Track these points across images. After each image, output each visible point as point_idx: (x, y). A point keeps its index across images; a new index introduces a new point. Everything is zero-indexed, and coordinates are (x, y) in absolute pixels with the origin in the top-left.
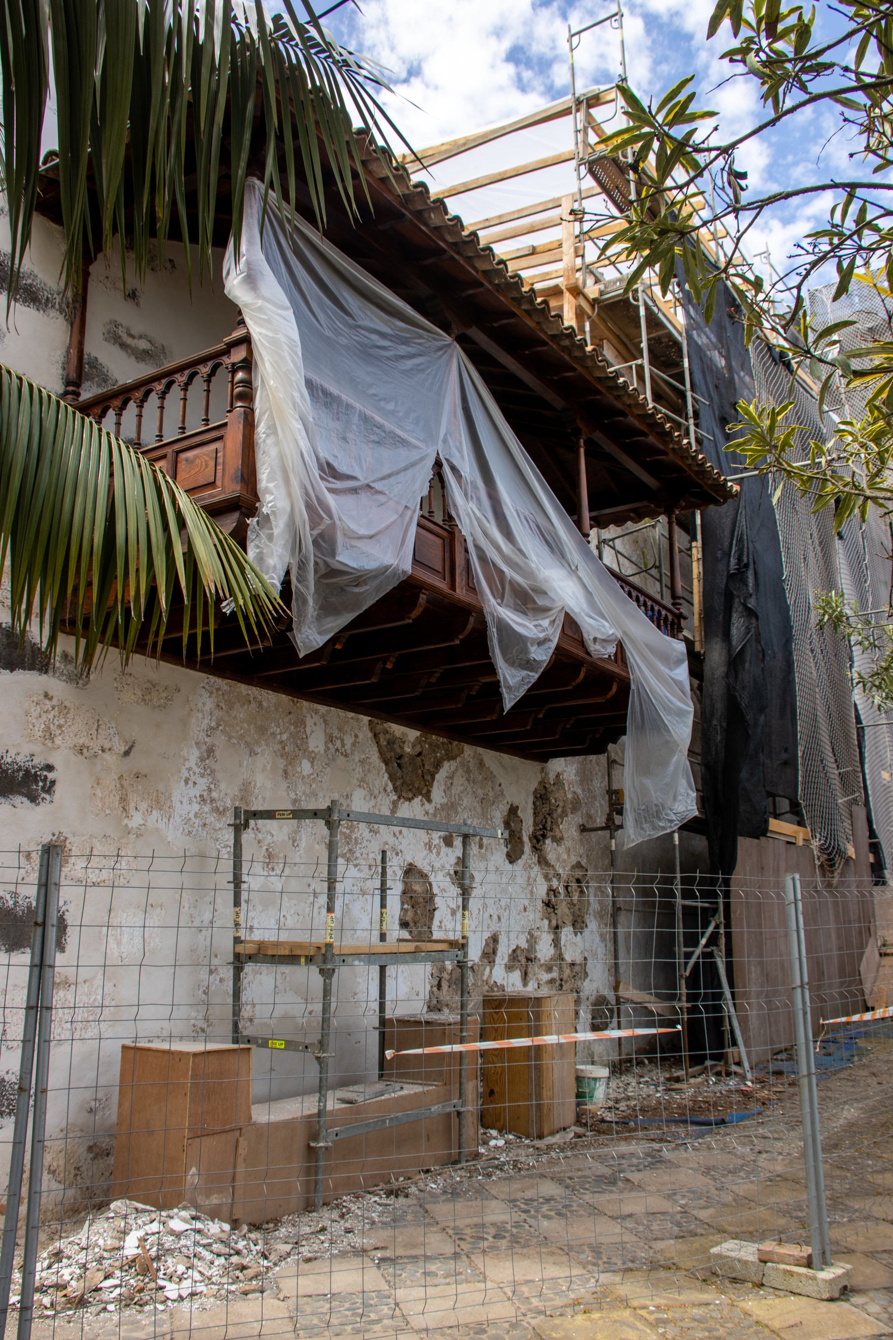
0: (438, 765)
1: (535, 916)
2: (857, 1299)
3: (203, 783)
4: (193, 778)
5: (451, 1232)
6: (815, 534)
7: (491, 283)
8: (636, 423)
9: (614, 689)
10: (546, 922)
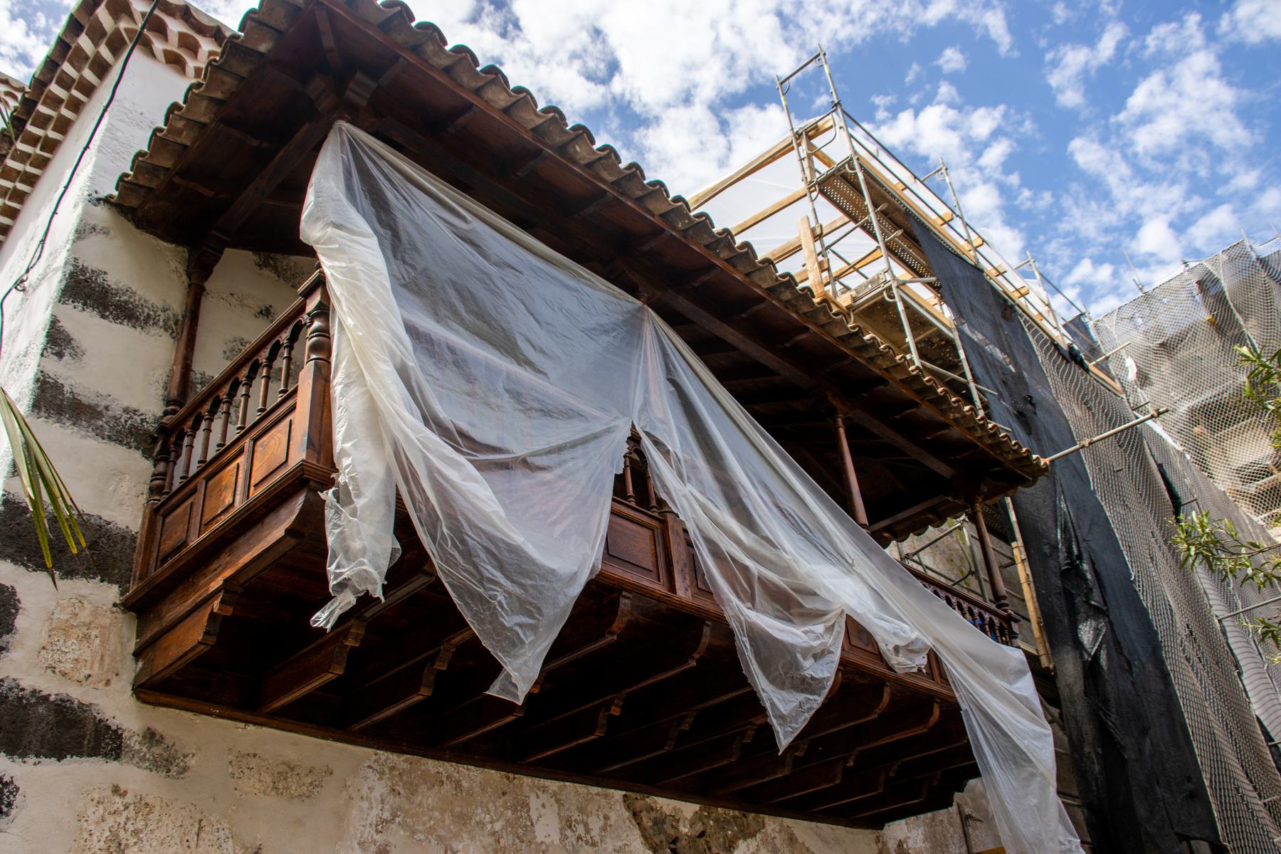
6: (1157, 532)
8: (906, 393)
9: (936, 711)
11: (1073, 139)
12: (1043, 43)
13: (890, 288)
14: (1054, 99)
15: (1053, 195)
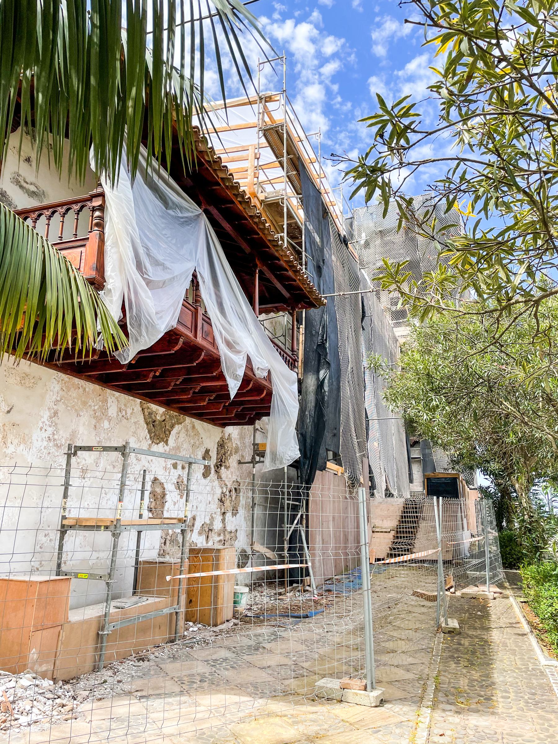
0: (172, 427)
1: (214, 507)
2: (387, 706)
3: (50, 430)
4: (45, 427)
5: (176, 680)
7: (224, 184)
8: (284, 264)
10: (219, 510)
11: (372, 76)
12: (377, 9)
13: (283, 199)
14: (371, 47)
15: (352, 106)
